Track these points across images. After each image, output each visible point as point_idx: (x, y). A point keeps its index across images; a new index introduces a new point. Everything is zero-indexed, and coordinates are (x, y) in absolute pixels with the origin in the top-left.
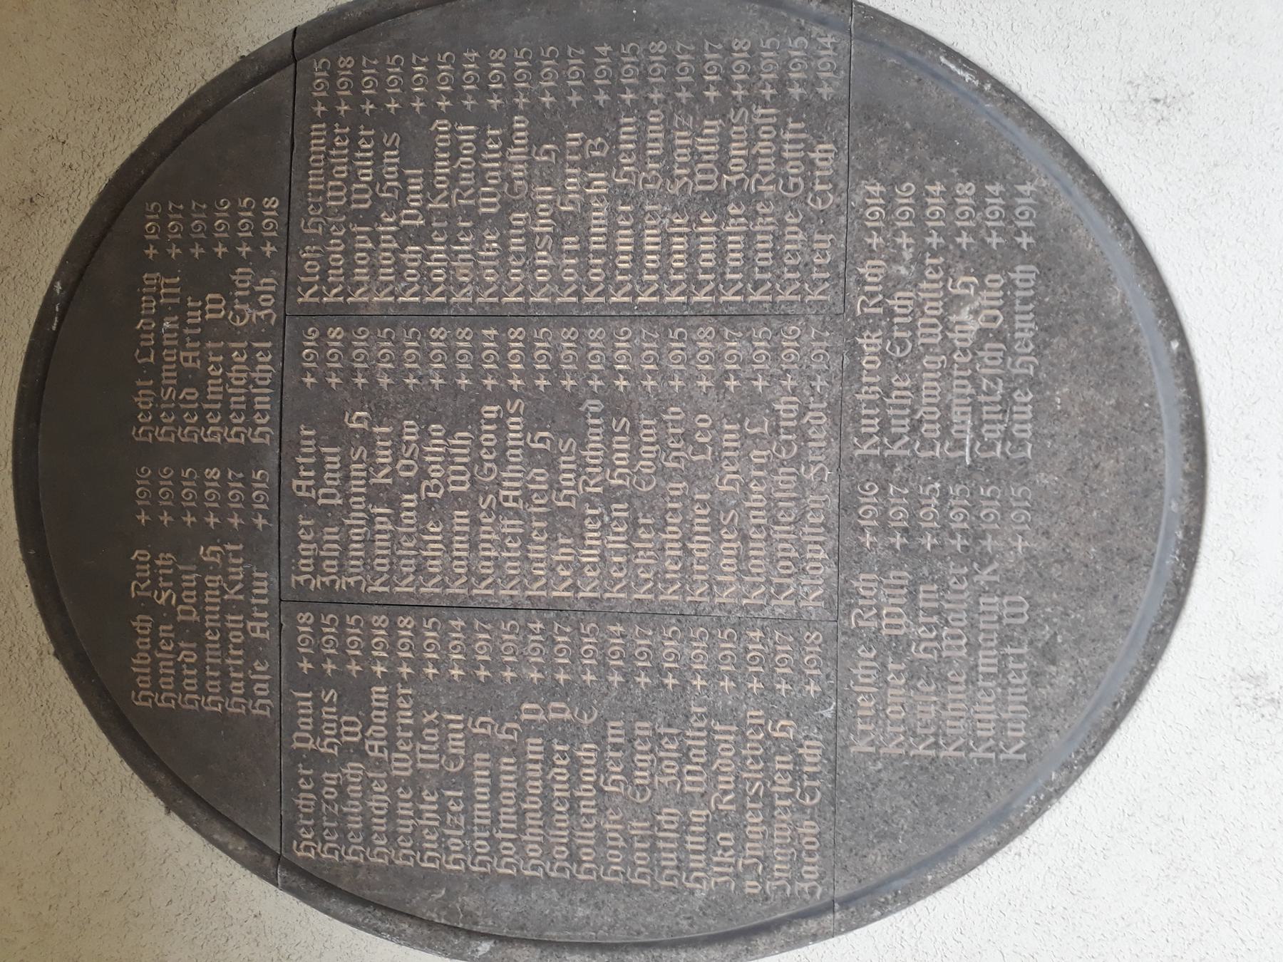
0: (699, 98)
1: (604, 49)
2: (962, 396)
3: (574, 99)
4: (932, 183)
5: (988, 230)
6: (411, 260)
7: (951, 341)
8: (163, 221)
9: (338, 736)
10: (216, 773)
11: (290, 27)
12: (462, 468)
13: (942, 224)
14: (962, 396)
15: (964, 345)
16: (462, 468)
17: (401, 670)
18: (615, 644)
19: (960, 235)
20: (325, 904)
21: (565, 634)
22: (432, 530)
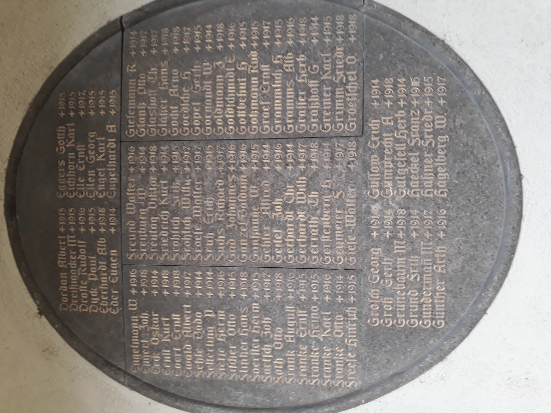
0: (226, 48)
1: (209, 26)
2: (388, 169)
3: (198, 48)
4: (374, 79)
5: (439, 97)
6: (174, 117)
7: (383, 145)
8: (67, 101)
9: (225, 333)
10: (104, 344)
11: (120, 15)
12: (153, 203)
13: (392, 96)
14: (388, 169)
15: (389, 146)
16: (153, 203)
17: (175, 293)
18: (302, 283)
19: (400, 101)
20: (178, 404)
21: (268, 278)
22: (277, 238)
